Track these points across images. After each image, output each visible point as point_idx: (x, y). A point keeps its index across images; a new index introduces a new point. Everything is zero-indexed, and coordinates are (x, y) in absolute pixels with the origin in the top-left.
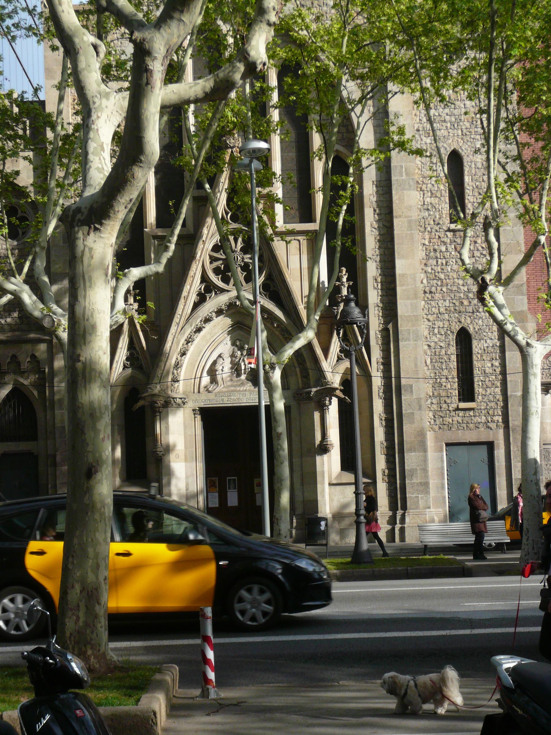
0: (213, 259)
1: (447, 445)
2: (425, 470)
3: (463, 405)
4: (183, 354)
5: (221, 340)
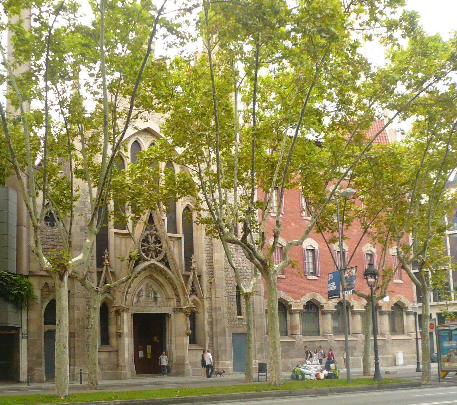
0: (142, 246)
1: (233, 334)
2: (225, 344)
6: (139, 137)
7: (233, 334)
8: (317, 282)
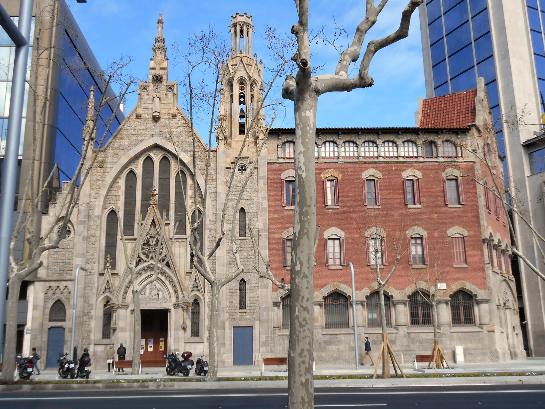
0: (143, 249)
1: (234, 327)
2: (224, 337)
3: (241, 310)
4: (128, 287)
5: (383, 248)
6: (151, 154)
7: (234, 327)
8: (342, 271)
